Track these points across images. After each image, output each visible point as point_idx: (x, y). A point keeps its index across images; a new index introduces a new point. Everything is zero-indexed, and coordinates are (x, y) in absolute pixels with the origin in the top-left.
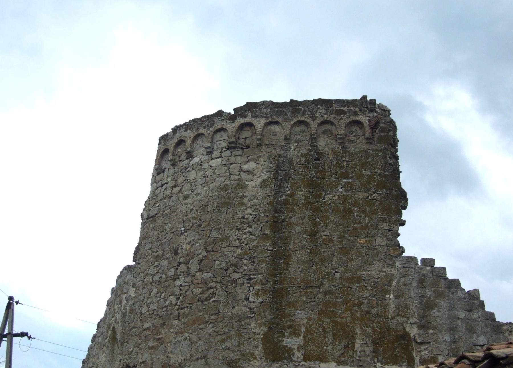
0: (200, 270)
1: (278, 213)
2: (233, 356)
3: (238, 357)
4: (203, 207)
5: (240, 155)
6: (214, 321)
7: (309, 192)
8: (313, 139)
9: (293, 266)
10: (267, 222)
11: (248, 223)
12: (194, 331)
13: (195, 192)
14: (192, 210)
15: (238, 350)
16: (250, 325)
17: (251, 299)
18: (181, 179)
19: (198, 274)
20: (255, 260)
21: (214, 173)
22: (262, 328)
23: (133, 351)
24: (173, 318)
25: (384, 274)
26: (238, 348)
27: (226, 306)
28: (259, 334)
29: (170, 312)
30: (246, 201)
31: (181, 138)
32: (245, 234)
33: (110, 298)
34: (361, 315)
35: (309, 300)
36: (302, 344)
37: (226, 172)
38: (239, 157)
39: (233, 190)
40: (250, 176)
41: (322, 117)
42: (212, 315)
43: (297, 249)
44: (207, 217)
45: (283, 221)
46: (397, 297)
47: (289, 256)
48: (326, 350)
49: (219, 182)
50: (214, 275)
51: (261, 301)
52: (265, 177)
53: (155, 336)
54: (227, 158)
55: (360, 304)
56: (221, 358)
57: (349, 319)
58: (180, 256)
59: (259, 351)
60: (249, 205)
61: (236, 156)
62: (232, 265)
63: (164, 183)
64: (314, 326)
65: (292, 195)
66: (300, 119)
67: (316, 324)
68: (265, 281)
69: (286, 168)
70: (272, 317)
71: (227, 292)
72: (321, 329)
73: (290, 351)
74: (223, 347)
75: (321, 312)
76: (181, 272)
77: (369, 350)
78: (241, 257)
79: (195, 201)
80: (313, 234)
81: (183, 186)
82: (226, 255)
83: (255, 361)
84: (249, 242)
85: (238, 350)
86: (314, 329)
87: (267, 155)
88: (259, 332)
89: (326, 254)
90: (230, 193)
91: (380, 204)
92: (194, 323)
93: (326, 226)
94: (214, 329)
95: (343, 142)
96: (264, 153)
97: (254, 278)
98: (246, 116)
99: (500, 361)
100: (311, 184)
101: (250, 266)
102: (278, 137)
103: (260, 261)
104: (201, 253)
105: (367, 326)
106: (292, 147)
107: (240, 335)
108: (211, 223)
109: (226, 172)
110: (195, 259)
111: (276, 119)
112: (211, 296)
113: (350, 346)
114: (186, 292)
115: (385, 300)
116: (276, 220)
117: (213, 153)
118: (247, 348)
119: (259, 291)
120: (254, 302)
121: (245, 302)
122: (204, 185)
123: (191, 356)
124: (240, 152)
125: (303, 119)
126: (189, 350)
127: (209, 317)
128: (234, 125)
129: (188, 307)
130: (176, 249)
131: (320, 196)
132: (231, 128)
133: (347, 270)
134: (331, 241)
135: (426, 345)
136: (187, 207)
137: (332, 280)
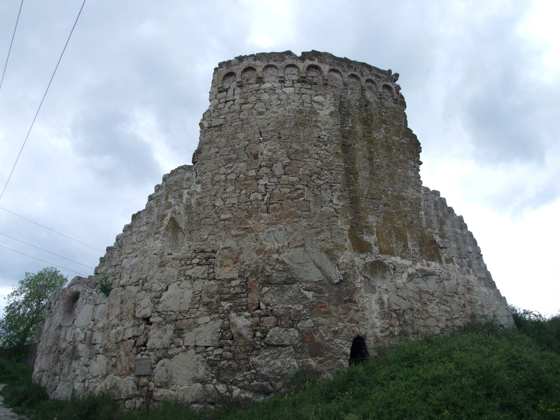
0: (285, 174)
1: (345, 138)
2: (329, 246)
3: (333, 247)
4: (281, 123)
5: (309, 89)
6: (307, 216)
7: (364, 128)
8: (363, 90)
9: (361, 181)
10: (338, 144)
11: (324, 142)
12: (288, 223)
13: (271, 110)
14: (269, 124)
15: (332, 242)
16: (337, 222)
17: (335, 202)
18: (252, 99)
19: (284, 177)
20: (333, 172)
21: (289, 98)
22: (346, 226)
23: (208, 238)
24: (261, 211)
25: (415, 197)
26: (331, 240)
27: (315, 205)
28: (345, 230)
29: (257, 206)
30: (319, 124)
31: (250, 66)
32: (322, 150)
34: (408, 224)
35: (376, 209)
36: (376, 241)
37: (299, 99)
38: (309, 90)
39: (308, 114)
40: (320, 107)
41: (367, 75)
42: (304, 211)
43: (361, 168)
44: (287, 132)
45: (350, 145)
46: (426, 214)
47: (357, 173)
48: (392, 247)
49: (294, 106)
50: (300, 180)
51: (342, 204)
52: (333, 110)
53: (240, 226)
54: (299, 89)
55: (406, 216)
56: (318, 247)
57: (402, 226)
58: (260, 160)
59: (348, 244)
60: (323, 128)
61: (306, 89)
62: (315, 173)
64: (382, 228)
65: (353, 127)
66: (354, 73)
67: (383, 227)
68: (343, 189)
69: (347, 107)
70: (352, 218)
71: (314, 194)
72: (387, 231)
73: (369, 245)
74: (319, 238)
75: (385, 219)
76: (265, 174)
77: (417, 249)
78: (322, 168)
79: (272, 117)
81: (255, 104)
82: (308, 164)
83: (347, 251)
84: (326, 157)
85: (332, 242)
86: (382, 231)
87: (332, 93)
88: (345, 228)
89: (380, 176)
90: (305, 117)
91: (408, 147)
92: (287, 217)
93: (378, 155)
94: (308, 223)
95: (381, 98)
96: (330, 91)
97: (335, 186)
98: (314, 60)
101: (330, 175)
102: (338, 82)
103: (337, 173)
104: (284, 160)
105: (413, 232)
106: (349, 92)
107: (331, 229)
108: (290, 137)
109: (299, 99)
110: (278, 164)
111: (336, 68)
112: (300, 195)
114: (273, 190)
115: (420, 215)
116: (345, 144)
117: (284, 83)
118: (338, 240)
119: (340, 197)
120: (337, 205)
121: (331, 204)
122: (279, 106)
123: (289, 244)
124: (309, 86)
125: (356, 73)
126: (286, 239)
127: (302, 213)
128: (303, 64)
129: (277, 203)
130: (254, 155)
131: (371, 133)
132: (301, 66)
133: (394, 190)
134: (382, 167)
136: (263, 121)
137: (387, 195)
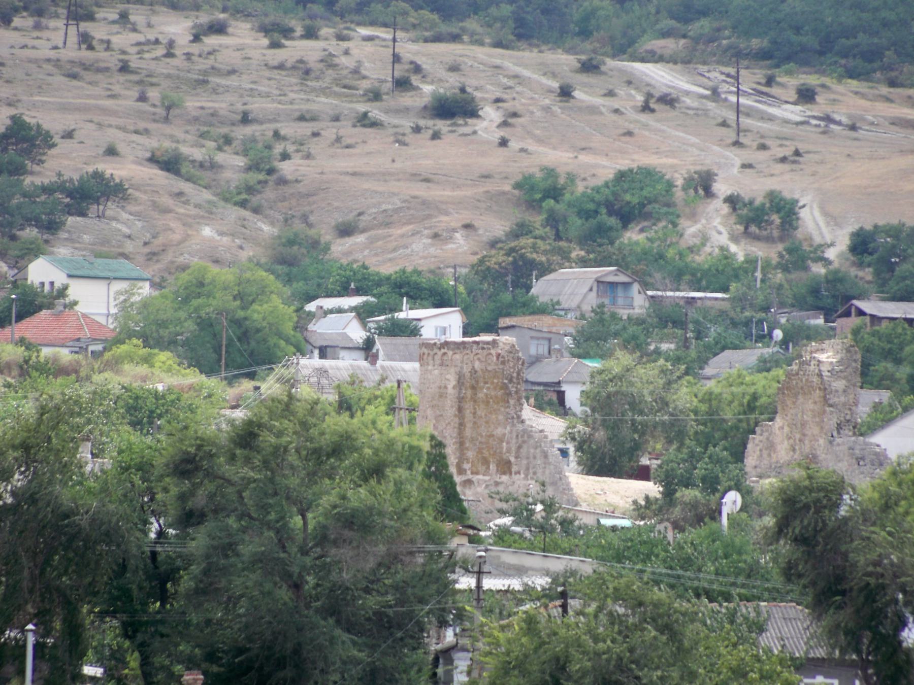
33: (31, 261)
63: (349, 314)
80: (475, 413)
99: (81, 669)
100: (473, 388)
113: (488, 468)
135: (899, 130)
